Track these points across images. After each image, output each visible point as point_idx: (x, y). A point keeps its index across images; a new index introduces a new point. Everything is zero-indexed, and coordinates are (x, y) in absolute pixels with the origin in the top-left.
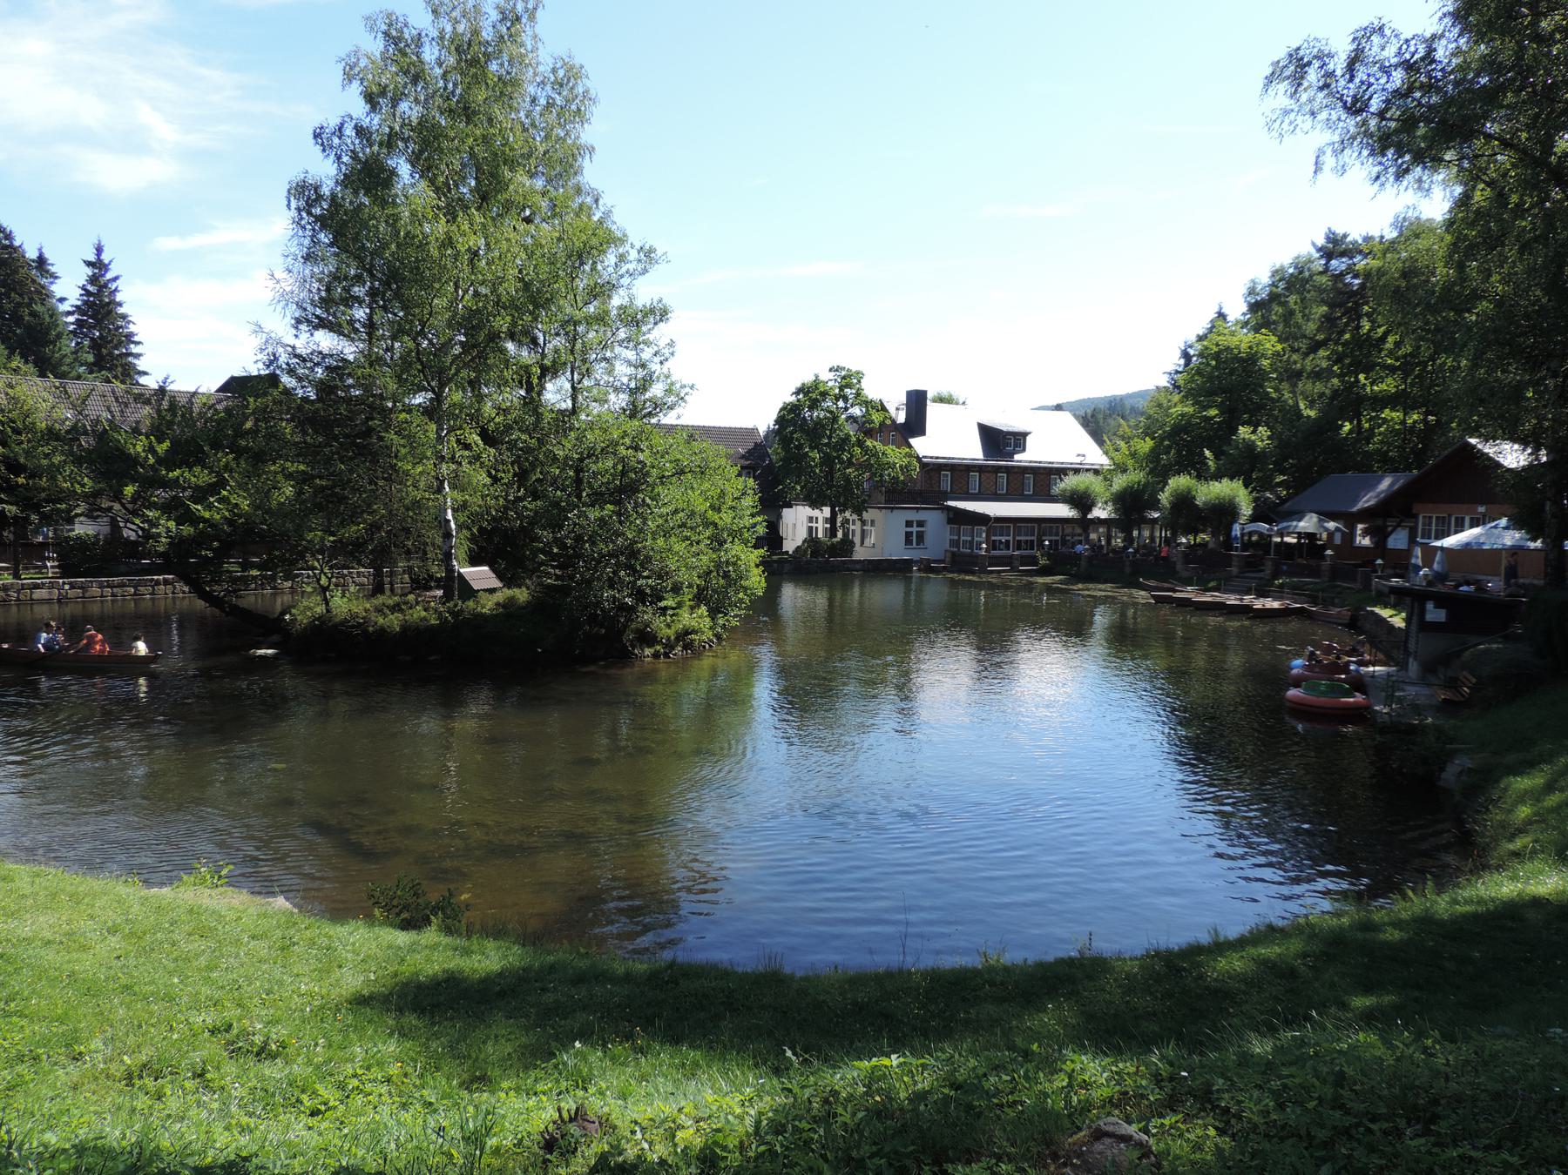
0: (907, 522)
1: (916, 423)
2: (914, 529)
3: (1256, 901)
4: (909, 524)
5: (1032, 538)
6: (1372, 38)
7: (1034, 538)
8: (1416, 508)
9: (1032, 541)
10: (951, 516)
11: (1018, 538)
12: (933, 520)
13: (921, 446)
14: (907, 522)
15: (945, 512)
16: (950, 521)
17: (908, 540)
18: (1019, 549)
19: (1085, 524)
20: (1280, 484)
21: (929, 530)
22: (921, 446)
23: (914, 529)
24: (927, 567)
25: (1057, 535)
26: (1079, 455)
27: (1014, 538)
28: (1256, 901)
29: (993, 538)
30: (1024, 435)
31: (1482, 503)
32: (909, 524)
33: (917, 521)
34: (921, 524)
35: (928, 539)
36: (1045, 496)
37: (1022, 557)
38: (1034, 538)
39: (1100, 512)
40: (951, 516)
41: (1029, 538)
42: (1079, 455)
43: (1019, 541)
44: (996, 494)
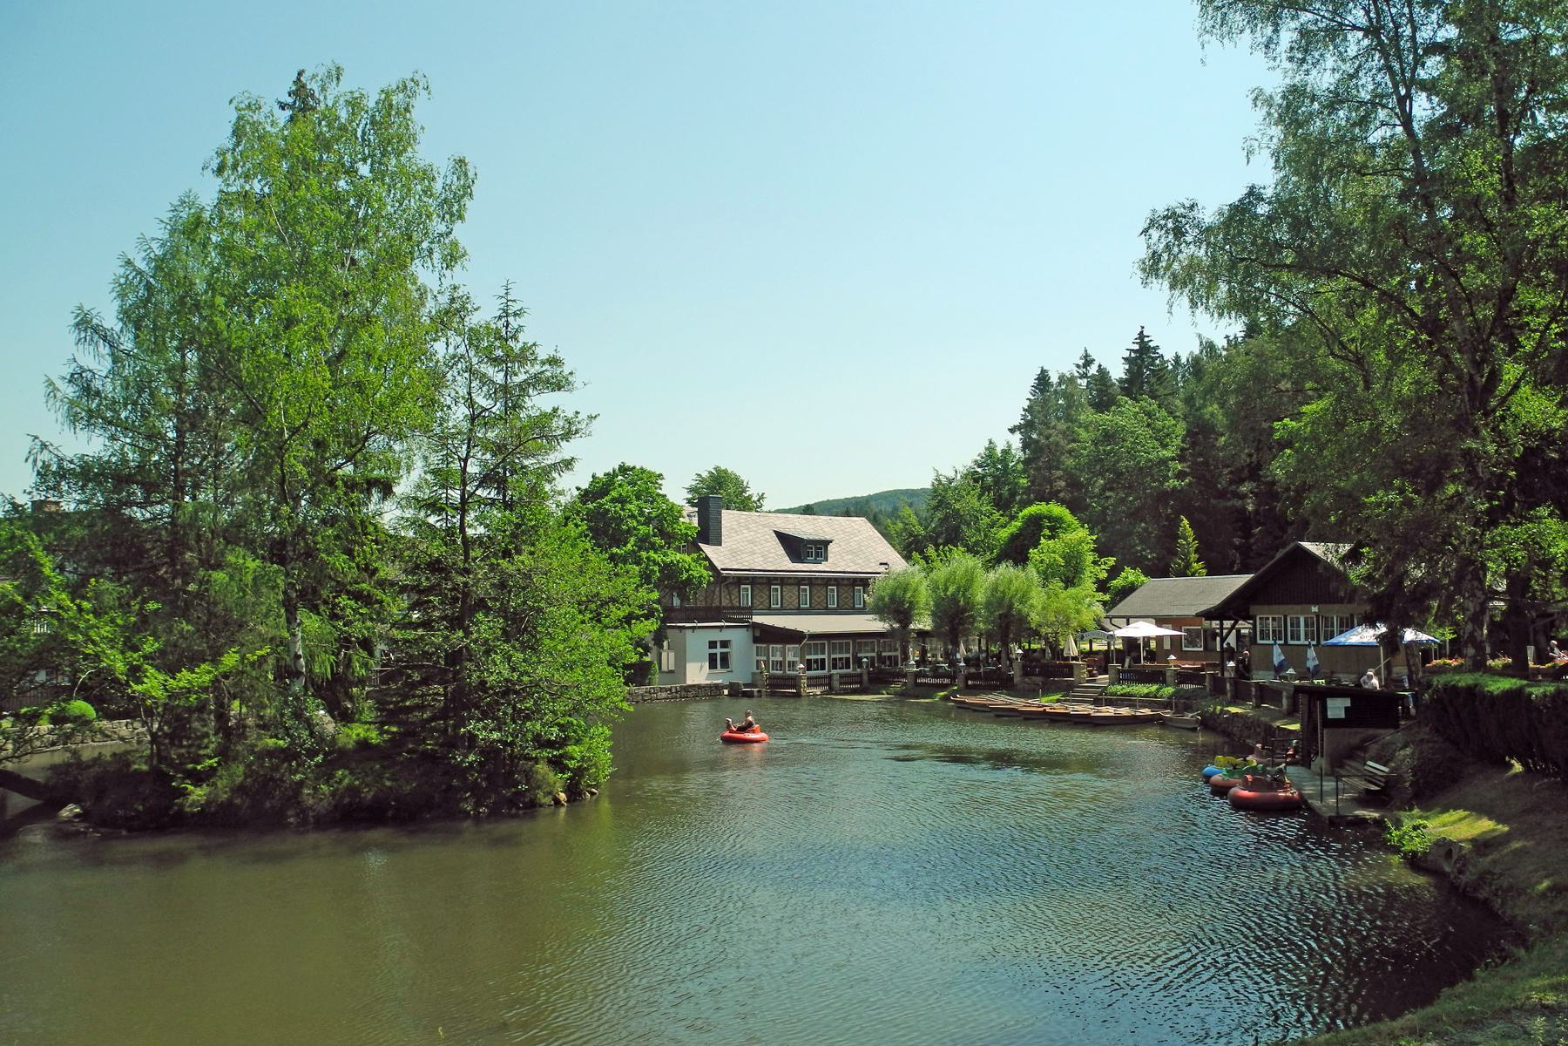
0: (710, 642)
1: (709, 532)
2: (718, 650)
3: (1203, 48)
4: (712, 644)
5: (847, 656)
6: (1151, 231)
7: (850, 655)
8: (1253, 609)
9: (848, 659)
10: (758, 634)
11: (833, 656)
12: (739, 639)
13: (718, 555)
14: (710, 642)
15: (750, 630)
16: (756, 640)
17: (713, 665)
18: (835, 667)
19: (901, 635)
20: (303, 495)
21: (735, 652)
22: (718, 555)
23: (718, 650)
24: (736, 691)
25: (874, 651)
26: (27, 460)
27: (829, 657)
28: (1203, 48)
29: (808, 657)
30: (827, 543)
31: (1315, 603)
32: (712, 644)
33: (721, 642)
34: (725, 644)
35: (734, 660)
36: (848, 608)
37: (842, 676)
38: (850, 655)
39: (924, 623)
40: (758, 634)
41: (820, 657)
42: (27, 460)
43: (835, 659)
44: (799, 608)
